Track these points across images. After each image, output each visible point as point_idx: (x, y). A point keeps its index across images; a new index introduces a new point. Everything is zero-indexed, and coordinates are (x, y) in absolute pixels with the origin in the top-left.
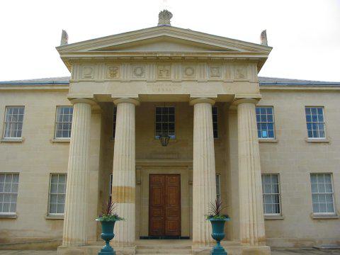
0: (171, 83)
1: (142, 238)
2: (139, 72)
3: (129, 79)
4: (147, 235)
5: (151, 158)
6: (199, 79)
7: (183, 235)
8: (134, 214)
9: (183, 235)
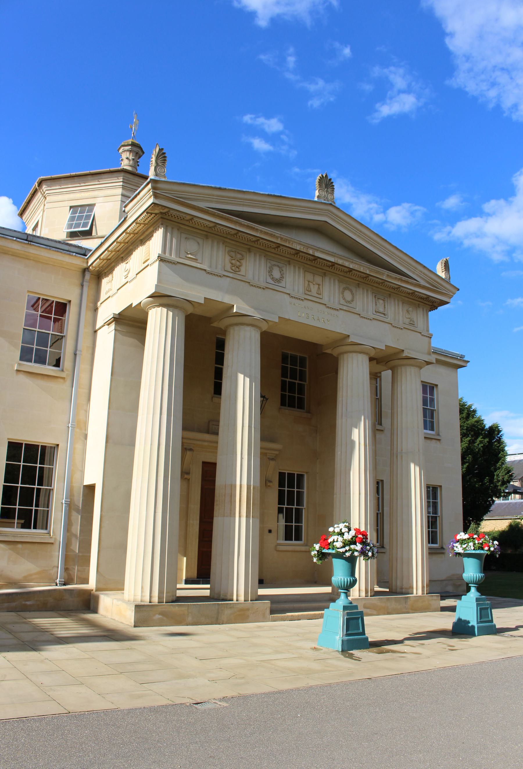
4: (341, 593)
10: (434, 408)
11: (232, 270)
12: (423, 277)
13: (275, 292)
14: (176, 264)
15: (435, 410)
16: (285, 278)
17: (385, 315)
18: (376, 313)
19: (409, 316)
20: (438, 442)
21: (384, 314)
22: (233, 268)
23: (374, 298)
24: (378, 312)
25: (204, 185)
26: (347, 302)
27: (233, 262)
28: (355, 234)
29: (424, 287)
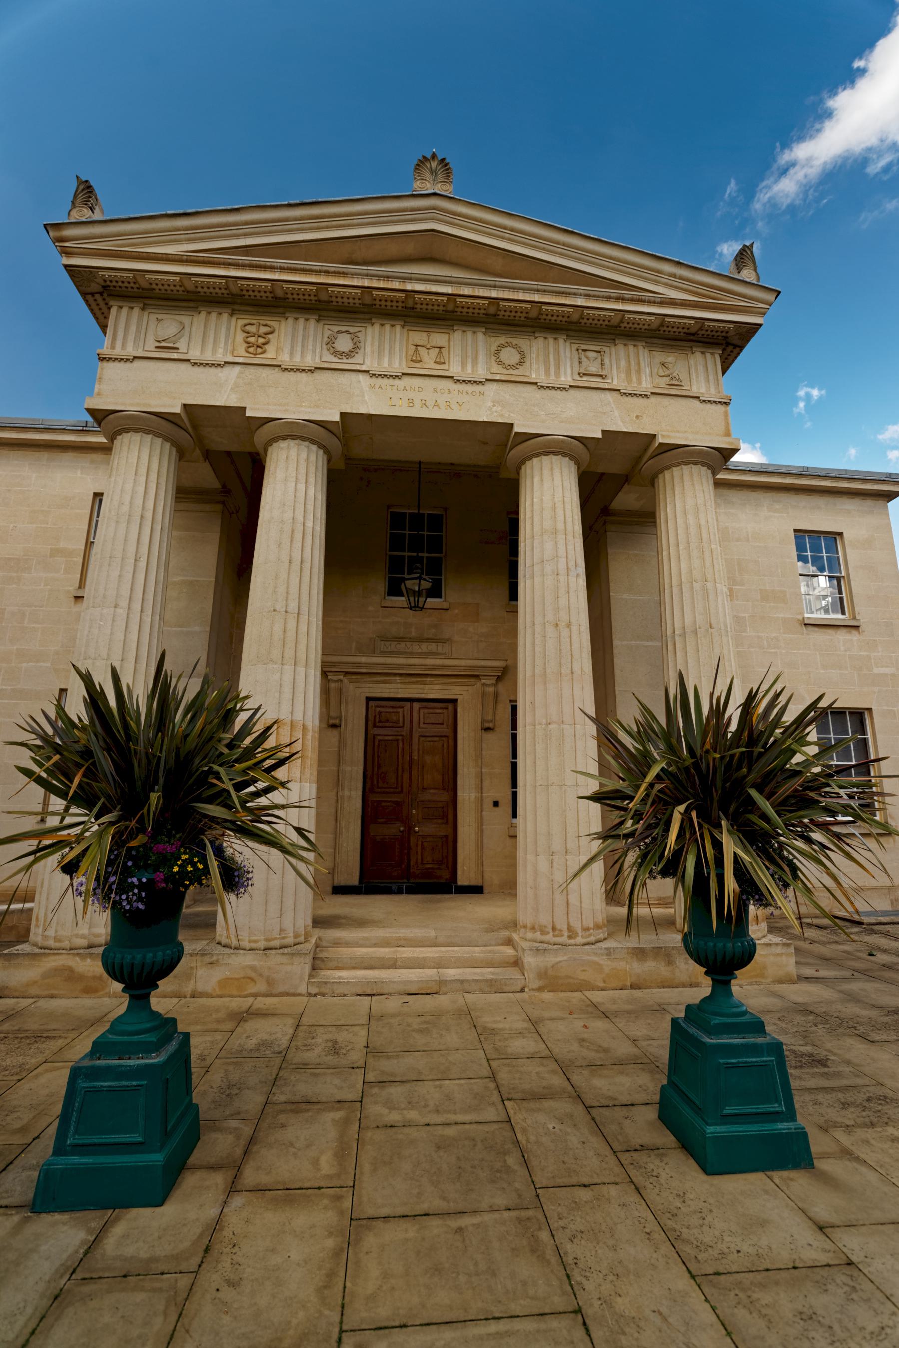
0: (448, 384)
1: (339, 890)
2: (344, 343)
3: (310, 361)
4: (355, 880)
5: (373, 652)
6: (542, 380)
7: (462, 880)
8: (324, 522)
9: (462, 880)
10: (841, 573)
11: (250, 353)
12: (681, 285)
13: (337, 373)
14: (133, 360)
15: (843, 577)
16: (362, 350)
17: (604, 379)
18: (581, 377)
19: (667, 373)
20: (854, 632)
21: (601, 376)
22: (251, 350)
23: (575, 353)
24: (584, 374)
25: (152, 214)
26: (509, 368)
27: (252, 340)
28: (503, 238)
29: (684, 304)
